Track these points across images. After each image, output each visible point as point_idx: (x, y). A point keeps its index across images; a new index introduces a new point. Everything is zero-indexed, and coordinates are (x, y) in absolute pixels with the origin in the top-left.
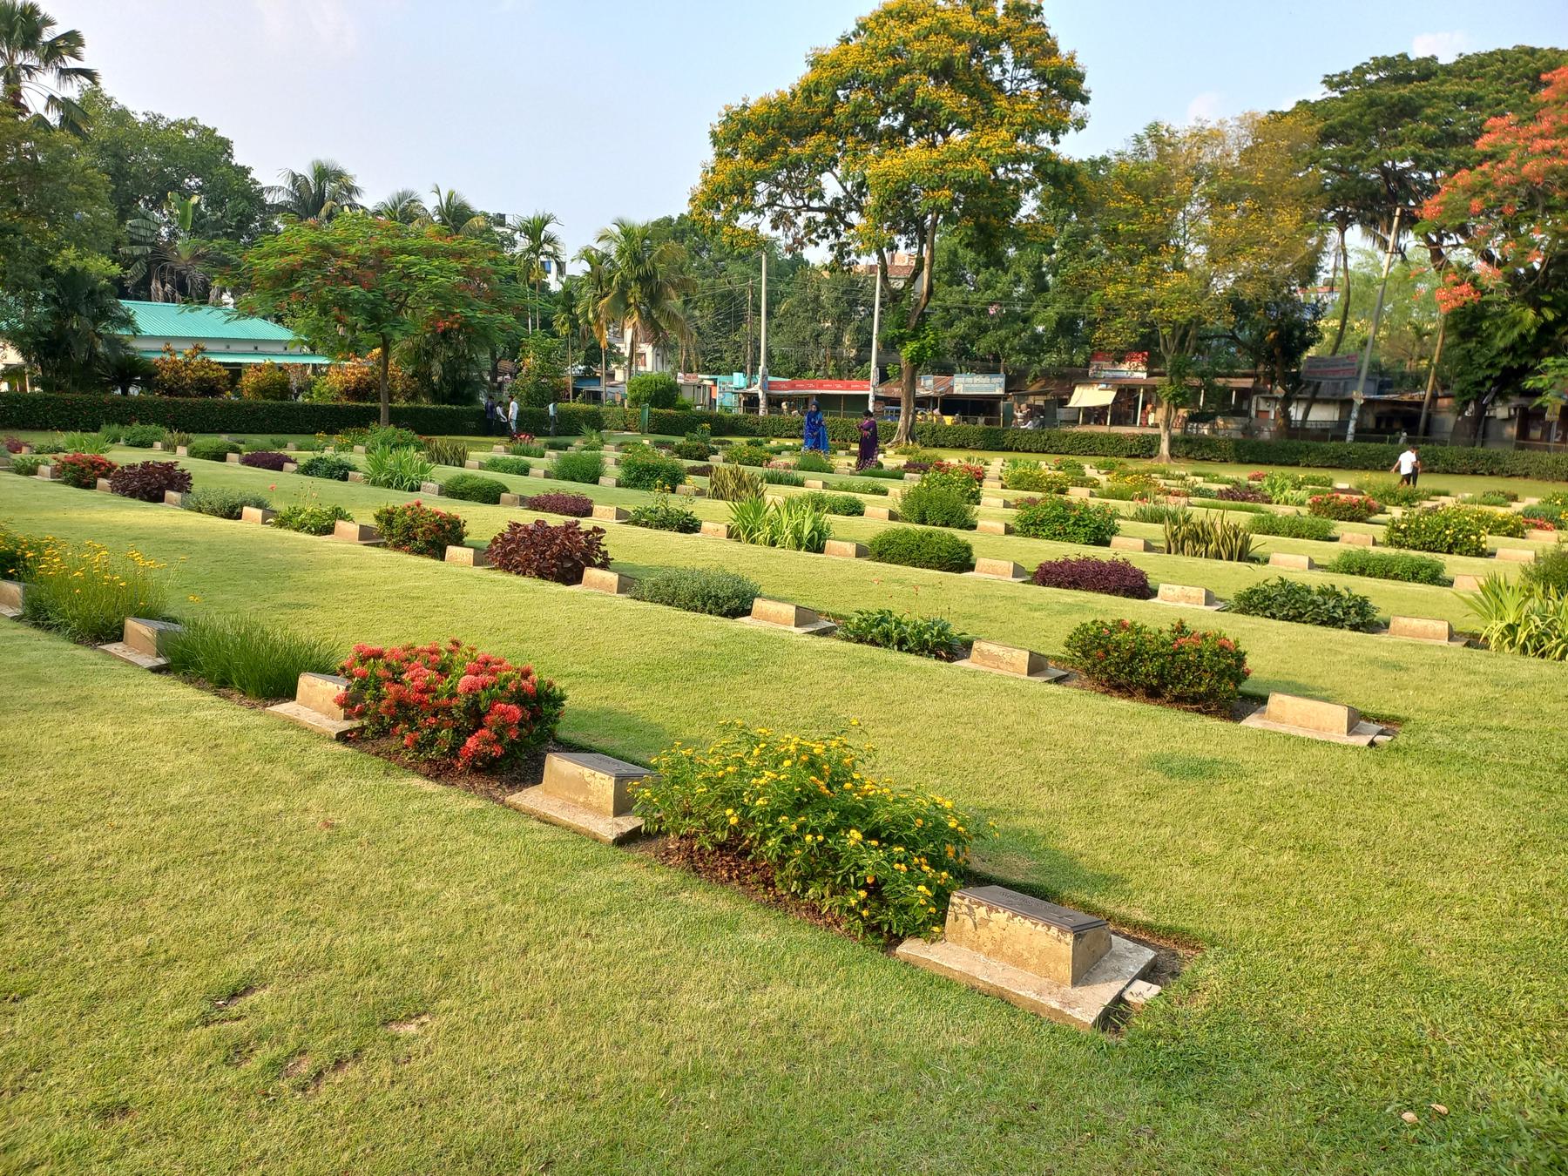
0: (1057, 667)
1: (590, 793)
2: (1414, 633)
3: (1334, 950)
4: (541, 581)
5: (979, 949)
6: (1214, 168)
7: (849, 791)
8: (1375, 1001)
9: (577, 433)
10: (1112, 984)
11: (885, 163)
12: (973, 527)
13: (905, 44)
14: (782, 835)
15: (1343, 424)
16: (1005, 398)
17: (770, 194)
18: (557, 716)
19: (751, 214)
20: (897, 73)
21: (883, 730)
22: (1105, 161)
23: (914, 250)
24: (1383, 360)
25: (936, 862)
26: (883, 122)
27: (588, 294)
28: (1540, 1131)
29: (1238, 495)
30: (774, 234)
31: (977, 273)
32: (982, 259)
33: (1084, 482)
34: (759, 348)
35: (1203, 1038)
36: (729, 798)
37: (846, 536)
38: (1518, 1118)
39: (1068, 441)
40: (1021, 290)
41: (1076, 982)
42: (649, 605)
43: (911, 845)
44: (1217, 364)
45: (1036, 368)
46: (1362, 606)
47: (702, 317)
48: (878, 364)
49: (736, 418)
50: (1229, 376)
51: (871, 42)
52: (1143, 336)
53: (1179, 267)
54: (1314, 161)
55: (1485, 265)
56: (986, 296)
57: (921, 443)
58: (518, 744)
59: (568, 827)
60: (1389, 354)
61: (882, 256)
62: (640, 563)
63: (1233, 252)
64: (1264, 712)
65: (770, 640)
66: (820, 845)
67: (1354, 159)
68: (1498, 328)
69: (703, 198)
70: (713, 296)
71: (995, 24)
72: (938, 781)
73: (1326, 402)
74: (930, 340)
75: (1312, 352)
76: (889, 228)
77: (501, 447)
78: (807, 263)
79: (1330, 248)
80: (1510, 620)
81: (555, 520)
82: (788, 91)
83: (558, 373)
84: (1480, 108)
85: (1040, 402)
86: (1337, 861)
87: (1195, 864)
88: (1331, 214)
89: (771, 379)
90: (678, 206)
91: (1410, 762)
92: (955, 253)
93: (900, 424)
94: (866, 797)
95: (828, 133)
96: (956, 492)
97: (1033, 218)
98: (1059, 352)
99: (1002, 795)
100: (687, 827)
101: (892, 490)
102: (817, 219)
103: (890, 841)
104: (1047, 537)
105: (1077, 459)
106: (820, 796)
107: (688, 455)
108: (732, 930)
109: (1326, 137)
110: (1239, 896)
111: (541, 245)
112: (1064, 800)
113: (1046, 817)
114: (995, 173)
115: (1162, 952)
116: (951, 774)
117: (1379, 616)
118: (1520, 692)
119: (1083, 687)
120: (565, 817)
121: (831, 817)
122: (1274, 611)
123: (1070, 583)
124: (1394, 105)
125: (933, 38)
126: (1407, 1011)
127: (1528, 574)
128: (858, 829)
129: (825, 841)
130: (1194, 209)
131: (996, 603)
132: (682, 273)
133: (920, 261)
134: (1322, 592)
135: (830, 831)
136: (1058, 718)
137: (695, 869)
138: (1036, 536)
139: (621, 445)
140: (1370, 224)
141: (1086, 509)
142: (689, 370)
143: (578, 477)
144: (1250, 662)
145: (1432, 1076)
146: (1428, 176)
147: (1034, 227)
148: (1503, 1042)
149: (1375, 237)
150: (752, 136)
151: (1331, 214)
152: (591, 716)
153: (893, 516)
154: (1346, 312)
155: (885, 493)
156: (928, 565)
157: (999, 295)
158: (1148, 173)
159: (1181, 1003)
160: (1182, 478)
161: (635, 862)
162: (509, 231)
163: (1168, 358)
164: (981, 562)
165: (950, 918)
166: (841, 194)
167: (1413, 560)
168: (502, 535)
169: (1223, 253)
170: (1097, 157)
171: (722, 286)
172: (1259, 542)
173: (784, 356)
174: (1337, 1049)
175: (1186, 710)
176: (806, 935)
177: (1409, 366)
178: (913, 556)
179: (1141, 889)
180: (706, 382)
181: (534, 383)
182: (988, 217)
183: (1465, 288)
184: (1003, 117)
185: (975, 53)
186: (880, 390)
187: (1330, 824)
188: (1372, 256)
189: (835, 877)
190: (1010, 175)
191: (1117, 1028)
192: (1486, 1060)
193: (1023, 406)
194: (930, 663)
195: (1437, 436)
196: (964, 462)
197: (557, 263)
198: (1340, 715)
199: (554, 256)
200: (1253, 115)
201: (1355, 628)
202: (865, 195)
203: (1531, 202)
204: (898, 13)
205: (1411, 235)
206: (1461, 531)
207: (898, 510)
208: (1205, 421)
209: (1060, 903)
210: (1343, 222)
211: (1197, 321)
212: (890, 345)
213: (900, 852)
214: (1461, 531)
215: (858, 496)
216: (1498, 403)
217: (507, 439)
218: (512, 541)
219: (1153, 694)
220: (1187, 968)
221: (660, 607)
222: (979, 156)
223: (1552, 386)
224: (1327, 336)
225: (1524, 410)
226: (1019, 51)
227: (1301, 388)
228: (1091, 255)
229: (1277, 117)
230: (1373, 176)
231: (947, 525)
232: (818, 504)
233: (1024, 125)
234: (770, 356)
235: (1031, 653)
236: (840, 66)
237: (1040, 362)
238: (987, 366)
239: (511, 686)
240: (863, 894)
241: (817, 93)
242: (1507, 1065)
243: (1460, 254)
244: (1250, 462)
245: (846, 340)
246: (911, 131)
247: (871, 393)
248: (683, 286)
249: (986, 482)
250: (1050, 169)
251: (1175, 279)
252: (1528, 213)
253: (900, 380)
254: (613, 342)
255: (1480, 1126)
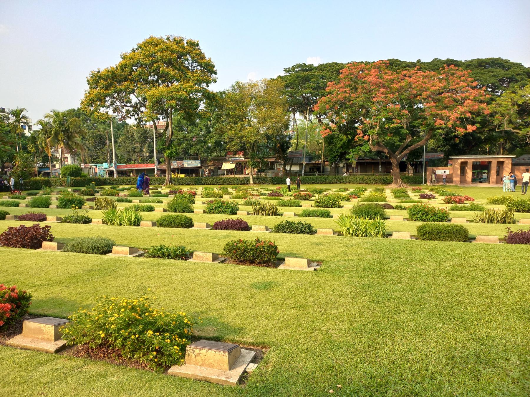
0: (222, 257)
1: (44, 333)
2: (324, 233)
3: (308, 340)
4: (23, 249)
5: (197, 364)
6: (256, 95)
7: (147, 316)
8: (320, 355)
9: (40, 188)
10: (242, 367)
11: (152, 92)
12: (193, 212)
13: (155, 53)
14: (123, 337)
15: (301, 171)
16: (201, 167)
17: (111, 101)
18: (29, 304)
19: (105, 108)
20: (153, 63)
21: (162, 289)
22: (224, 92)
23: (166, 120)
24: (309, 151)
25: (181, 336)
26: (150, 78)
27: (42, 137)
28: (366, 386)
29: (274, 194)
30: (114, 115)
31: (187, 127)
32: (189, 123)
33: (228, 194)
34: (112, 154)
35: (271, 379)
36: (101, 327)
37: (148, 219)
38: (360, 384)
39: (222, 180)
40: (203, 133)
41: (230, 369)
42: (70, 254)
43: (172, 332)
44: (264, 154)
45: (210, 157)
46: (309, 226)
47: (89, 144)
48: (157, 158)
49: (106, 179)
50: (267, 158)
51: (143, 52)
52: (241, 147)
53: (250, 125)
54: (284, 94)
55: (332, 123)
56: (191, 135)
57: (174, 184)
58: (10, 319)
59: (34, 349)
60: (311, 150)
61: (154, 123)
62: (67, 237)
63: (264, 121)
64: (284, 263)
65: (120, 261)
66: (137, 339)
67: (295, 93)
68: (338, 141)
69: (86, 102)
70: (93, 136)
71: (184, 49)
72: (182, 305)
73: (296, 164)
74: (174, 149)
75: (290, 150)
76: (156, 113)
77: (7, 197)
78: (128, 124)
79: (291, 119)
80: (348, 227)
81: (29, 224)
82: (115, 67)
83: (31, 166)
84: (325, 79)
85: (212, 168)
86: (307, 309)
87: (266, 318)
88: (291, 109)
89: (118, 164)
90: (76, 105)
91: (325, 274)
92: (180, 121)
93: (167, 178)
94: (154, 317)
95: (131, 81)
96: (186, 200)
97: (203, 110)
98: (217, 152)
99: (204, 306)
100: (86, 340)
101: (164, 201)
102: (130, 110)
103: (164, 331)
104: (217, 213)
105: (225, 186)
106: (137, 320)
107: (86, 194)
108: (104, 378)
109: (286, 86)
110: (280, 327)
111: (20, 119)
112: (224, 304)
113: (219, 311)
114: (190, 96)
115: (258, 351)
116: (187, 301)
117: (314, 229)
118: (352, 248)
119: (230, 263)
120: (33, 345)
121: (141, 327)
122: (285, 230)
123: (225, 228)
124: (304, 78)
125: (164, 52)
126: (329, 356)
127: (351, 212)
128: (151, 330)
129: (139, 337)
130: (252, 108)
131: (201, 237)
132: (80, 128)
133: (168, 124)
134: (298, 224)
135: (141, 333)
136: (222, 275)
137: (89, 356)
138: (213, 213)
139: (59, 192)
140: (301, 112)
141: (228, 203)
142: (86, 163)
143: (40, 206)
144: (279, 248)
145: (336, 375)
146: (315, 98)
147: (204, 113)
148: (355, 360)
149: (303, 116)
150: (102, 81)
151: (291, 109)
152: (45, 302)
153: (165, 210)
154: (298, 138)
155: (162, 202)
156: (178, 226)
157: (195, 134)
158: (237, 97)
159: (264, 369)
160: (258, 190)
161: (64, 358)
162: (6, 114)
163: (250, 153)
164: (195, 224)
165: (187, 355)
166: (138, 101)
167: (322, 211)
168: (5, 233)
169: (262, 121)
170: (222, 91)
171: (96, 132)
172: (280, 209)
173: (123, 157)
174: (310, 373)
175: (262, 266)
176: (134, 373)
177: (316, 153)
178: (172, 224)
179: (250, 331)
180: (93, 167)
181: (21, 171)
182: (189, 110)
183: (328, 130)
184: (190, 78)
185: (179, 57)
186: (158, 166)
187: (305, 297)
188: (303, 121)
189: (144, 349)
190: (194, 96)
191: (244, 382)
192: (351, 367)
193: (207, 170)
194: (179, 262)
195: (326, 173)
196: (189, 190)
197: (28, 126)
198: (305, 262)
199: (26, 123)
200: (265, 80)
201: (308, 233)
202: (146, 102)
203: (341, 106)
204: (151, 43)
205: (312, 115)
206: (334, 201)
207: (167, 208)
208: (263, 172)
209: (225, 341)
210: (294, 112)
211: (256, 142)
212: (160, 152)
213: (167, 335)
214: (334, 201)
215: (152, 204)
216: (340, 163)
217: (10, 193)
218: (10, 234)
219: (252, 262)
220: (265, 356)
221: (75, 254)
222: (183, 90)
223: (353, 157)
224: (294, 145)
225: (347, 164)
226: (193, 58)
227: (288, 160)
228: (223, 122)
229: (273, 80)
230: (301, 98)
231: (184, 212)
232: (137, 208)
233: (197, 80)
234: (117, 157)
235: (213, 254)
236: (133, 59)
237: (211, 156)
238: (195, 157)
239: (6, 296)
240: (155, 353)
241: (125, 68)
242: (356, 367)
243: (326, 121)
244: (276, 184)
245: (145, 150)
246: (160, 81)
247: (155, 168)
248: (80, 133)
249: (196, 196)
250: (207, 94)
251: (249, 129)
252: (341, 109)
253: (165, 163)
254: (54, 154)
255: (350, 389)
